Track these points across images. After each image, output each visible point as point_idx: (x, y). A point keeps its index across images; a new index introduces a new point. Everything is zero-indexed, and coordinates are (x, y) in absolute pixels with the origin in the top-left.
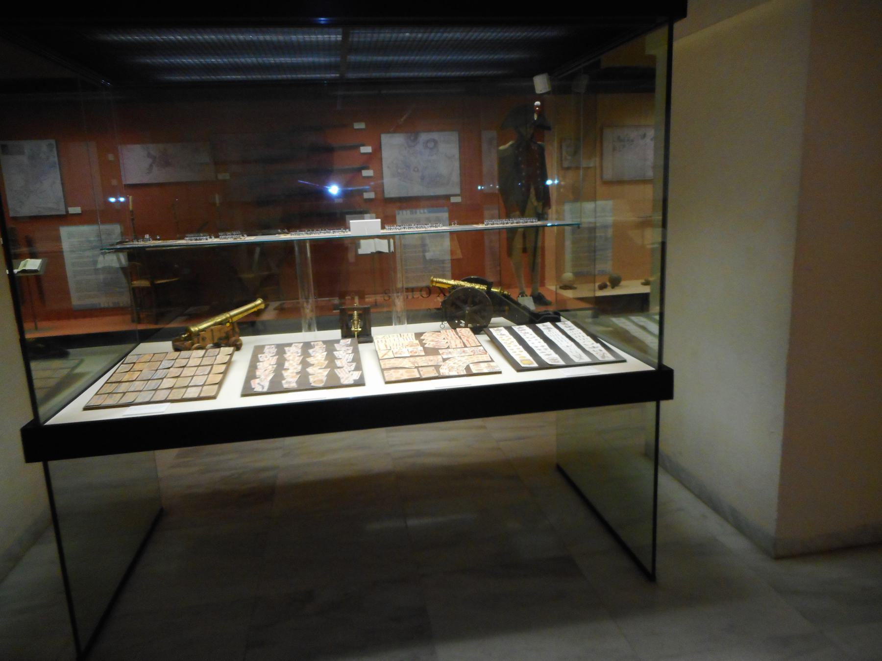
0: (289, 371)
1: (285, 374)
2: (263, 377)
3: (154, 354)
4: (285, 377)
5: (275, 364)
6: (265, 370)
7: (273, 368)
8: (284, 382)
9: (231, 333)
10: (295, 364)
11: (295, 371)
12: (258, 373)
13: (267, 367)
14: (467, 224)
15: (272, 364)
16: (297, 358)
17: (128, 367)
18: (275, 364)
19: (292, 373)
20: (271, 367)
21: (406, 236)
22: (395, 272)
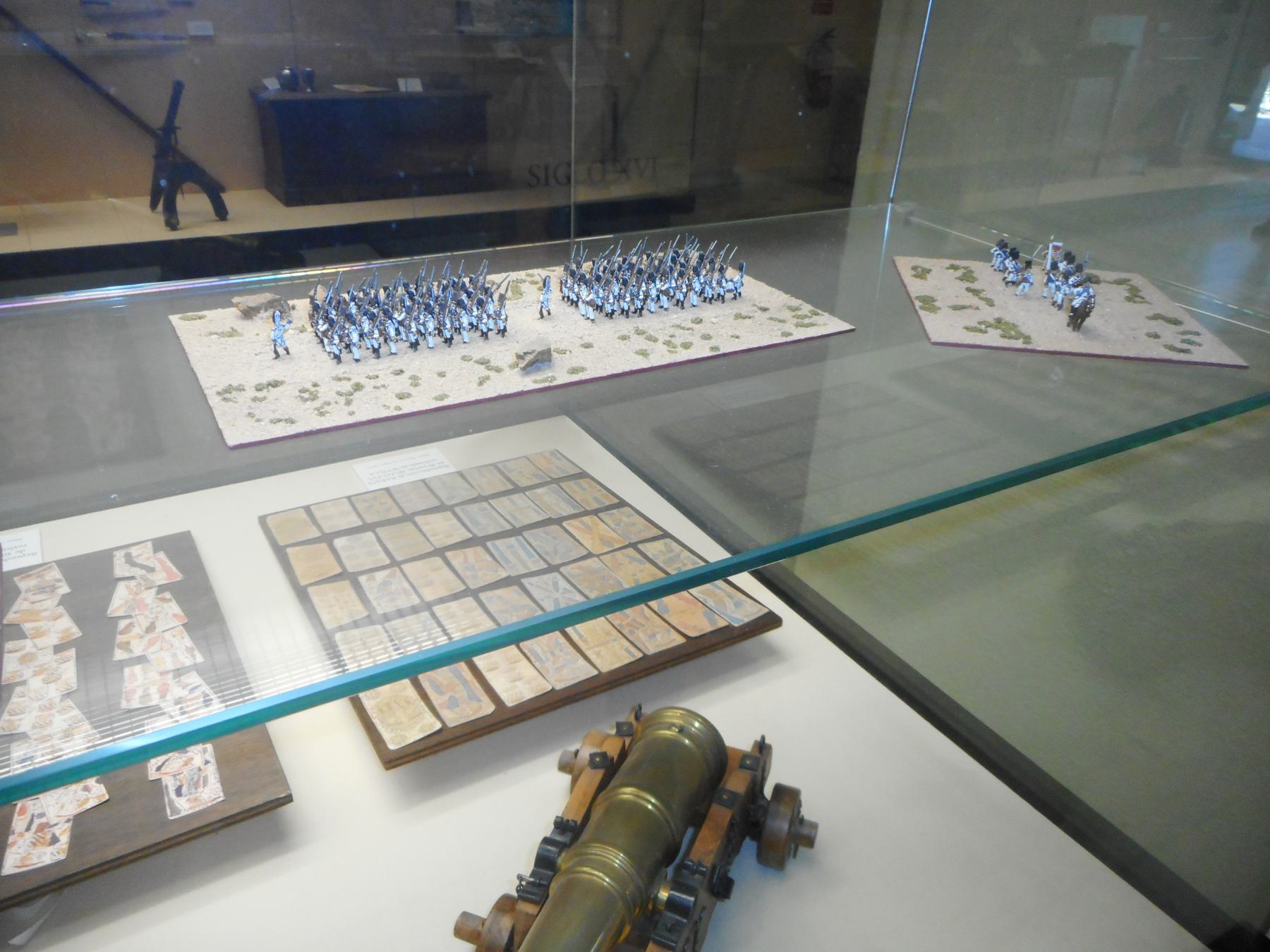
0: (53, 639)
1: (65, 626)
2: (149, 596)
3: (583, 475)
4: (61, 609)
5: (122, 664)
6: (151, 628)
7: (126, 646)
8: (64, 589)
9: (645, 335)
10: (35, 683)
11: (28, 645)
12: (627, 543)
13: (151, 643)
14: (552, 241)
15: (137, 669)
16: (25, 724)
17: (652, 549)
18: (122, 664)
19: (39, 634)
20: (138, 649)
21: (832, 340)
22: (353, 92)
